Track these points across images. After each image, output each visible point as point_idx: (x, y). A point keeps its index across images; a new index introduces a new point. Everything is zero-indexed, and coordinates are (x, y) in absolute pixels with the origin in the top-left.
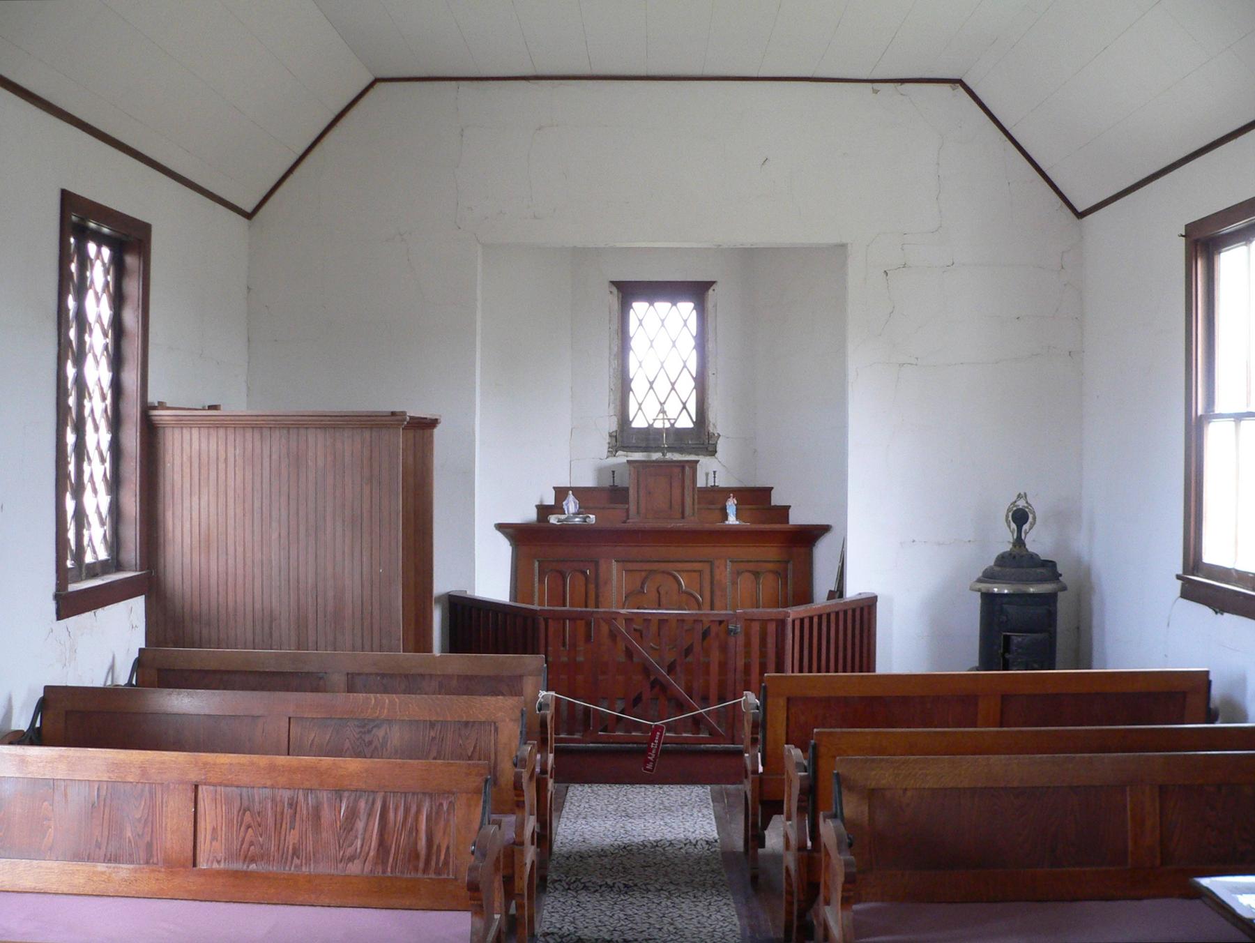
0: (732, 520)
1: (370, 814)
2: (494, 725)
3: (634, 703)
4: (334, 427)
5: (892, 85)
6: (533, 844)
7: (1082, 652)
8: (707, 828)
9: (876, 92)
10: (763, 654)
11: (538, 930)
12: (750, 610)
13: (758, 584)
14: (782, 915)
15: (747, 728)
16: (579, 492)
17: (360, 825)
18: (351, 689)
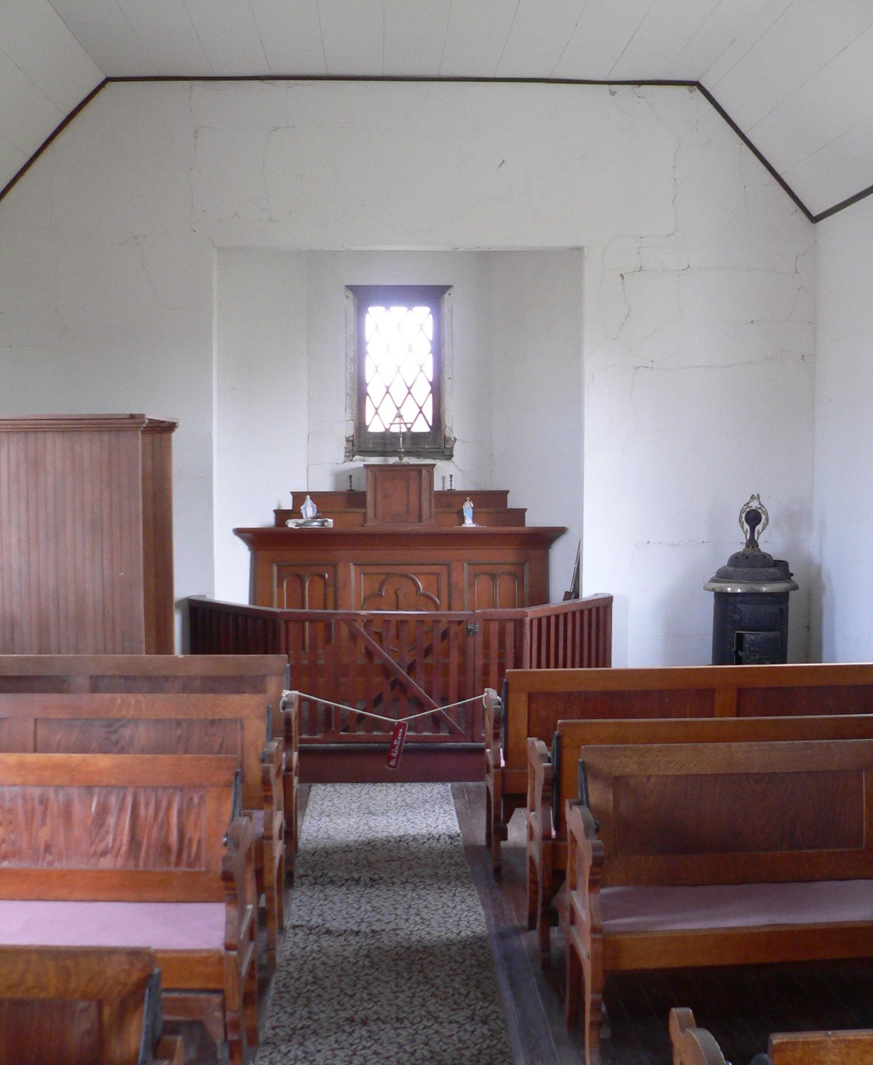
0: (469, 523)
1: (121, 810)
2: (239, 722)
3: (375, 703)
4: (73, 431)
5: (628, 86)
6: (280, 838)
7: (812, 647)
8: (449, 823)
9: (613, 93)
10: (501, 656)
11: (287, 923)
12: (488, 611)
13: (494, 586)
14: (527, 904)
15: (489, 724)
16: (316, 497)
17: (111, 820)
18: (95, 689)
